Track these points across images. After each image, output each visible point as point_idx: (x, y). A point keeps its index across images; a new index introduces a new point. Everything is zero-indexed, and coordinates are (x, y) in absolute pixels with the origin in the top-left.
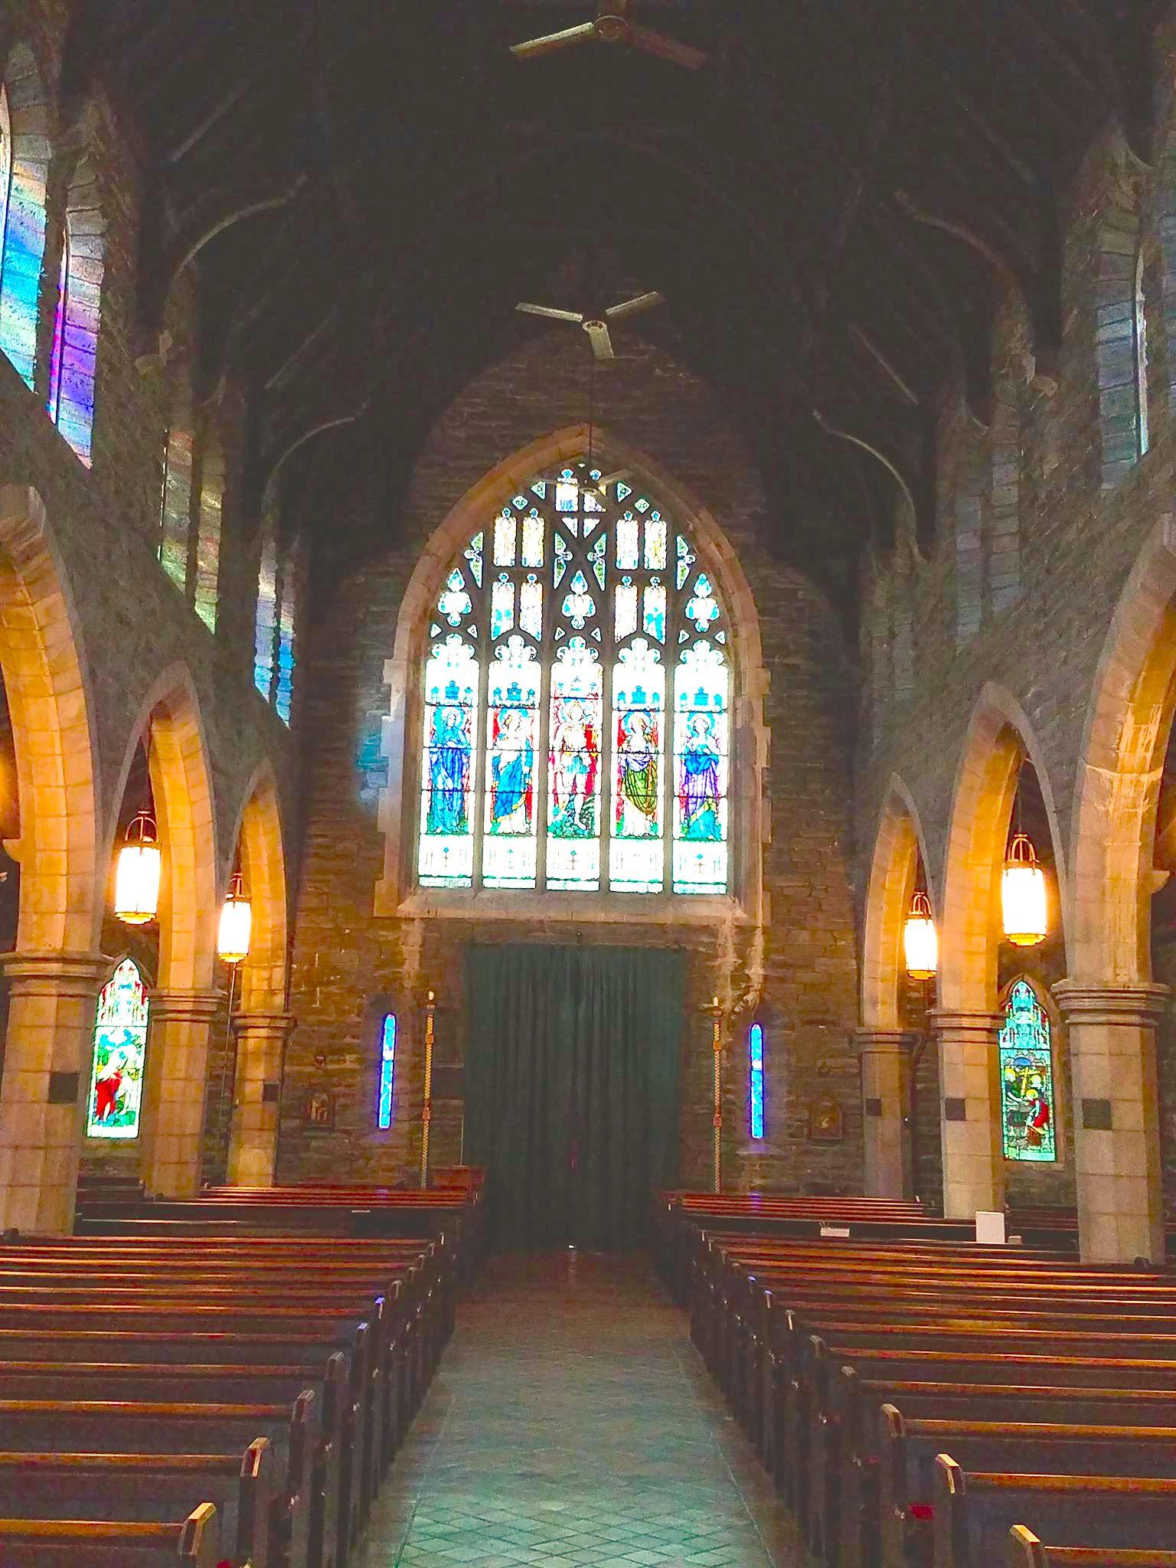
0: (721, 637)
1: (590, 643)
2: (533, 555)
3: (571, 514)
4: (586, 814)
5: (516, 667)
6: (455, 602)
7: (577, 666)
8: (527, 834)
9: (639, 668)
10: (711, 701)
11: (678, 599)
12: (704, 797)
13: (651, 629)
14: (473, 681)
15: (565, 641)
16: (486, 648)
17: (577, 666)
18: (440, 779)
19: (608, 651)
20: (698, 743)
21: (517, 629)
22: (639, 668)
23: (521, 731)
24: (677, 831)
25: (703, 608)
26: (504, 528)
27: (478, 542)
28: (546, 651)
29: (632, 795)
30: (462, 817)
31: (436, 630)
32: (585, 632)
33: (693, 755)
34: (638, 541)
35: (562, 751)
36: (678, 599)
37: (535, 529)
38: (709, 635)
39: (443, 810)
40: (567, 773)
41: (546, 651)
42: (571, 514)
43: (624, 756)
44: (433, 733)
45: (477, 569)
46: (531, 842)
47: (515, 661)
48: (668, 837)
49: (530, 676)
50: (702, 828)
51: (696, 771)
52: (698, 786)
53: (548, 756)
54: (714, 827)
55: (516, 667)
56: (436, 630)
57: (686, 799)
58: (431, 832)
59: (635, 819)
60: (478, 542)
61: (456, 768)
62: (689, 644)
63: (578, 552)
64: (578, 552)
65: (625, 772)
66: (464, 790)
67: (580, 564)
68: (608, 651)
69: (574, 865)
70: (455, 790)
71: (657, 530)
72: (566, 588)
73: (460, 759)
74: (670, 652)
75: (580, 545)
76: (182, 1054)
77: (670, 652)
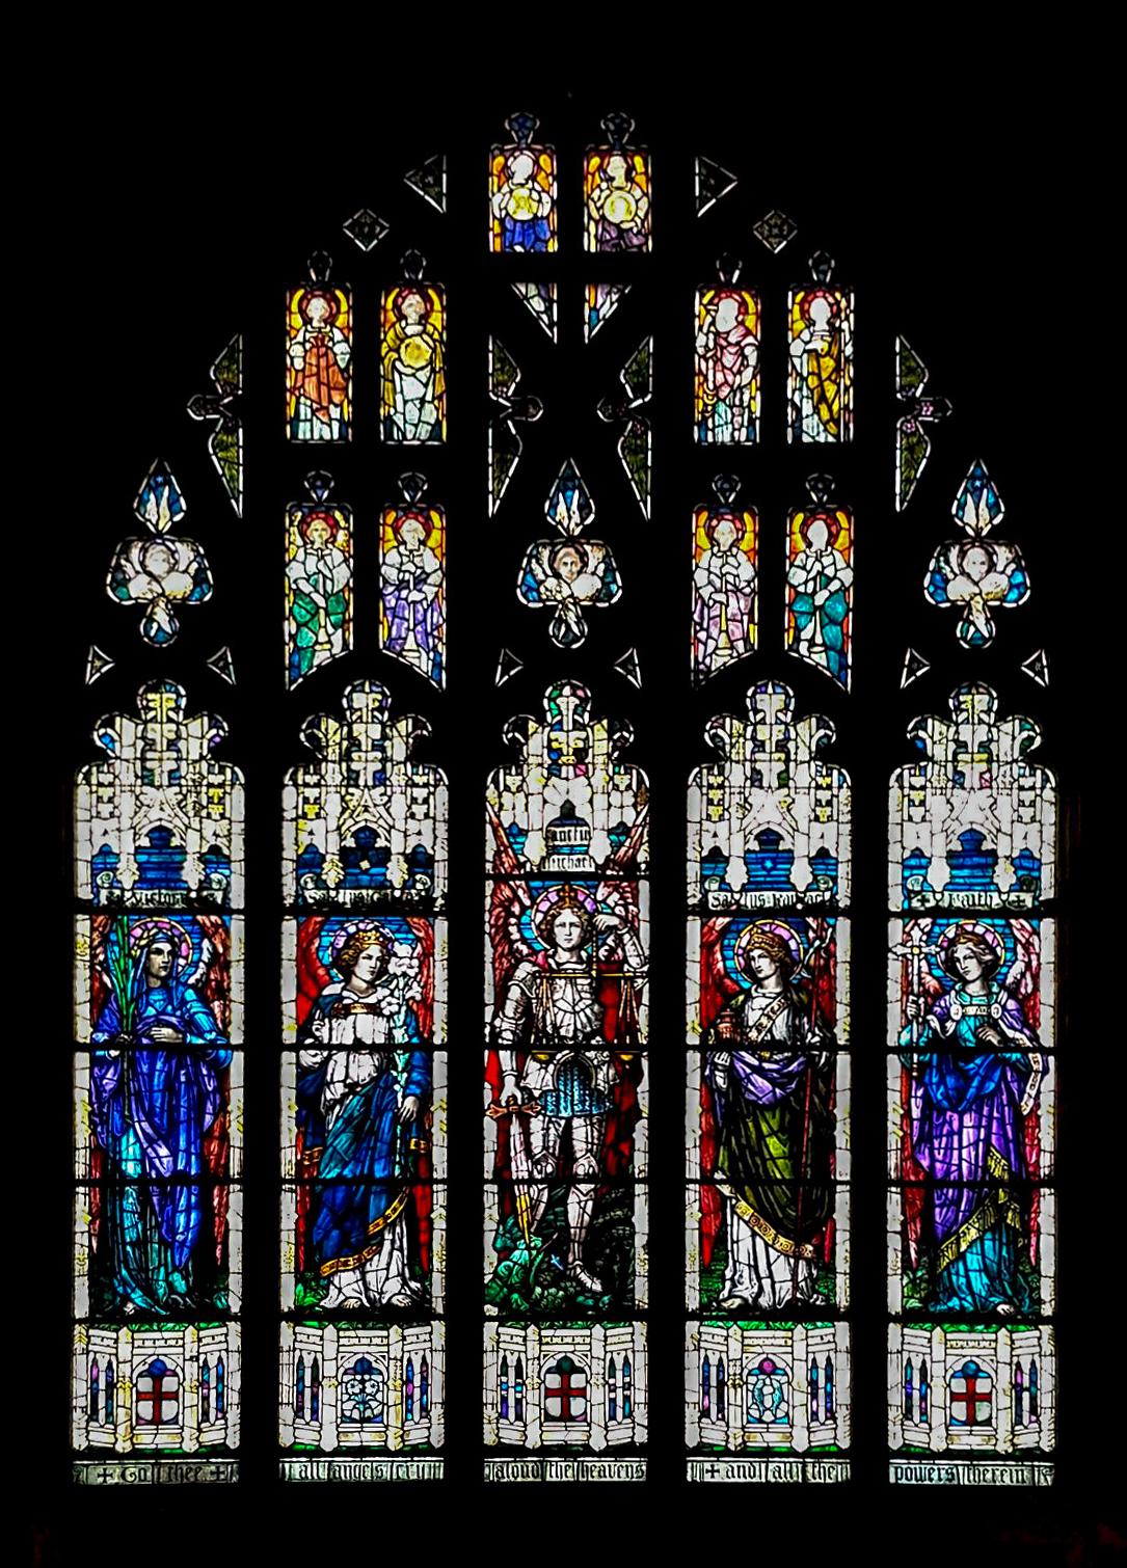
0: (1037, 669)
1: (608, 703)
2: (414, 404)
3: (536, 268)
4: (605, 1245)
5: (368, 794)
6: (161, 576)
7: (567, 790)
8: (416, 1313)
9: (772, 796)
10: (1005, 876)
11: (895, 554)
12: (982, 1184)
13: (815, 644)
14: (223, 822)
15: (527, 702)
16: (268, 736)
17: (567, 790)
18: (130, 1148)
19: (668, 735)
20: (964, 1010)
21: (367, 660)
22: (772, 796)
23: (370, 1019)
24: (896, 1293)
25: (979, 581)
26: (315, 324)
27: (226, 375)
28: (466, 739)
29: (748, 1176)
30: (207, 1271)
31: (97, 668)
32: (589, 667)
33: (947, 1050)
34: (777, 357)
35: (522, 1050)
36: (895, 554)
37: (416, 329)
38: (994, 666)
39: (141, 1244)
40: (542, 1120)
41: (466, 739)
42: (536, 268)
43: (722, 1059)
44: (101, 998)
45: (229, 462)
46: (427, 1343)
47: (366, 764)
48: (869, 1325)
49: (412, 817)
50: (979, 1283)
51: (957, 1102)
52: (966, 1144)
53: (469, 1076)
54: (1015, 1272)
55: (368, 794)
56: (97, 668)
57: (924, 1189)
58: (107, 1314)
59: (761, 1260)
60: (226, 375)
61: (182, 1111)
62: (934, 701)
63: (572, 401)
64: (572, 401)
65: (731, 1111)
66: (212, 1178)
67: (570, 439)
68: (668, 735)
69: (568, 1399)
70: (180, 1178)
71: (819, 323)
72: (527, 525)
73: (195, 1080)
74: (870, 745)
75: (570, 374)
76: (412, 388)
77: (870, 745)
